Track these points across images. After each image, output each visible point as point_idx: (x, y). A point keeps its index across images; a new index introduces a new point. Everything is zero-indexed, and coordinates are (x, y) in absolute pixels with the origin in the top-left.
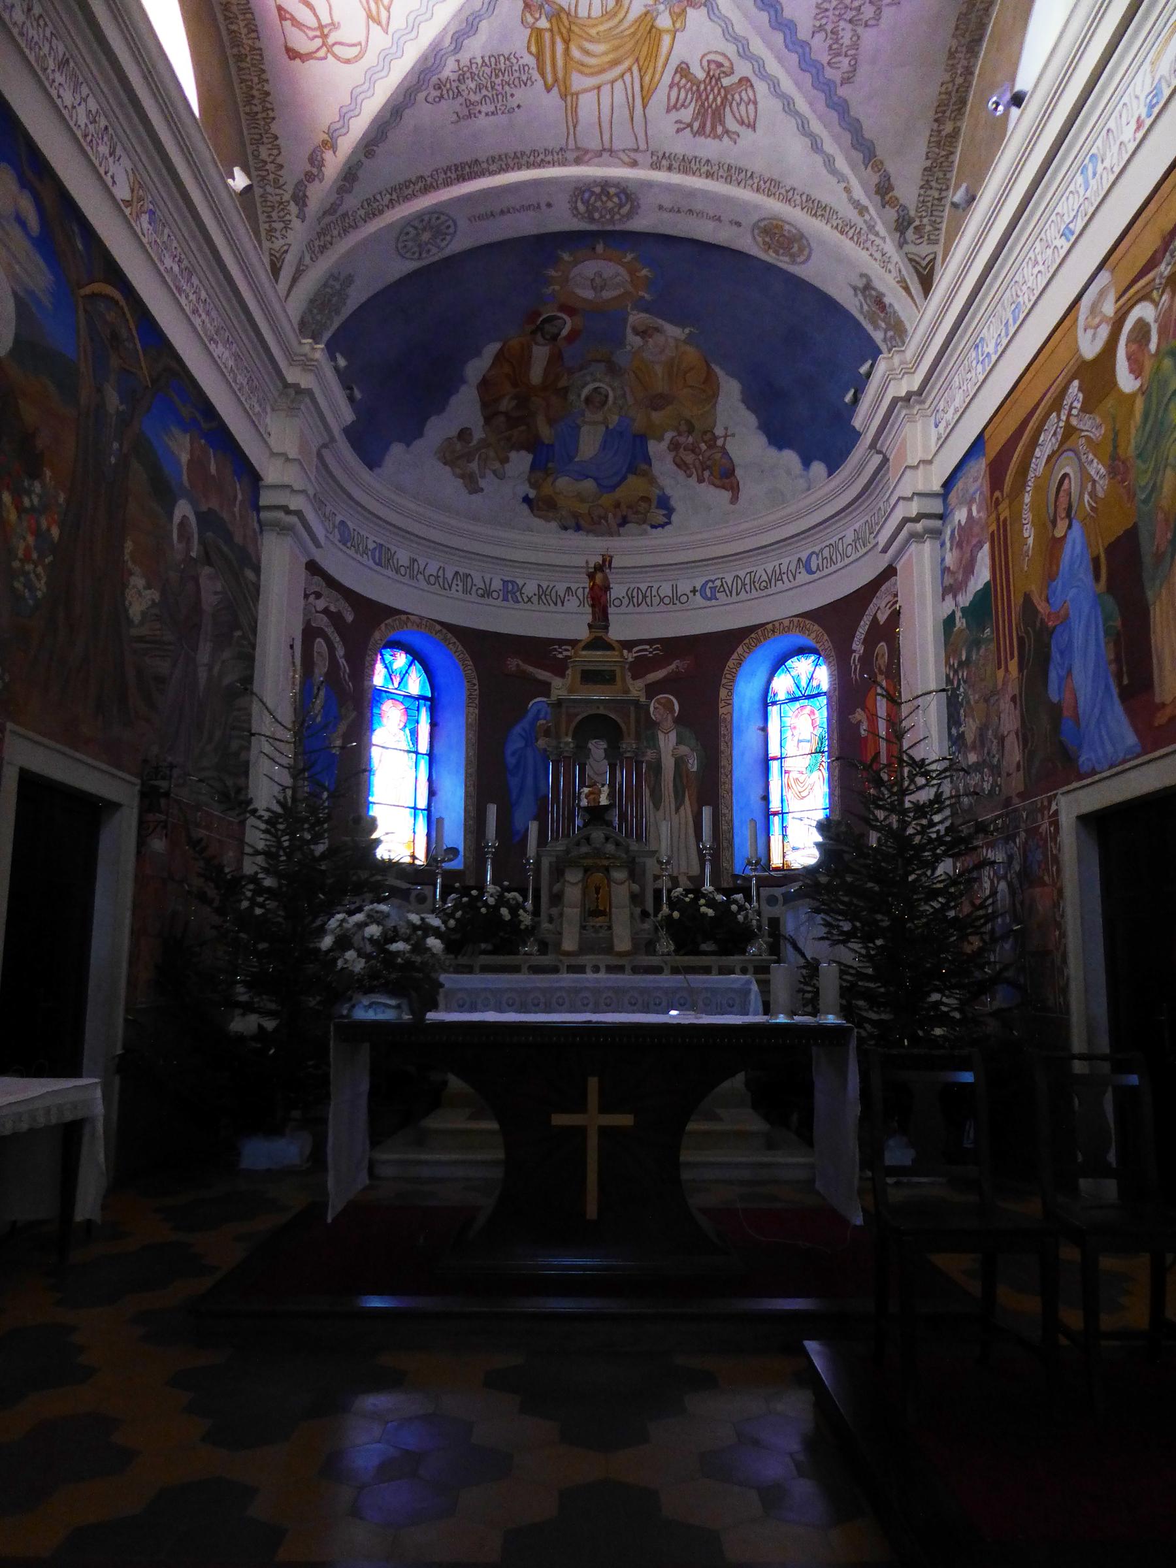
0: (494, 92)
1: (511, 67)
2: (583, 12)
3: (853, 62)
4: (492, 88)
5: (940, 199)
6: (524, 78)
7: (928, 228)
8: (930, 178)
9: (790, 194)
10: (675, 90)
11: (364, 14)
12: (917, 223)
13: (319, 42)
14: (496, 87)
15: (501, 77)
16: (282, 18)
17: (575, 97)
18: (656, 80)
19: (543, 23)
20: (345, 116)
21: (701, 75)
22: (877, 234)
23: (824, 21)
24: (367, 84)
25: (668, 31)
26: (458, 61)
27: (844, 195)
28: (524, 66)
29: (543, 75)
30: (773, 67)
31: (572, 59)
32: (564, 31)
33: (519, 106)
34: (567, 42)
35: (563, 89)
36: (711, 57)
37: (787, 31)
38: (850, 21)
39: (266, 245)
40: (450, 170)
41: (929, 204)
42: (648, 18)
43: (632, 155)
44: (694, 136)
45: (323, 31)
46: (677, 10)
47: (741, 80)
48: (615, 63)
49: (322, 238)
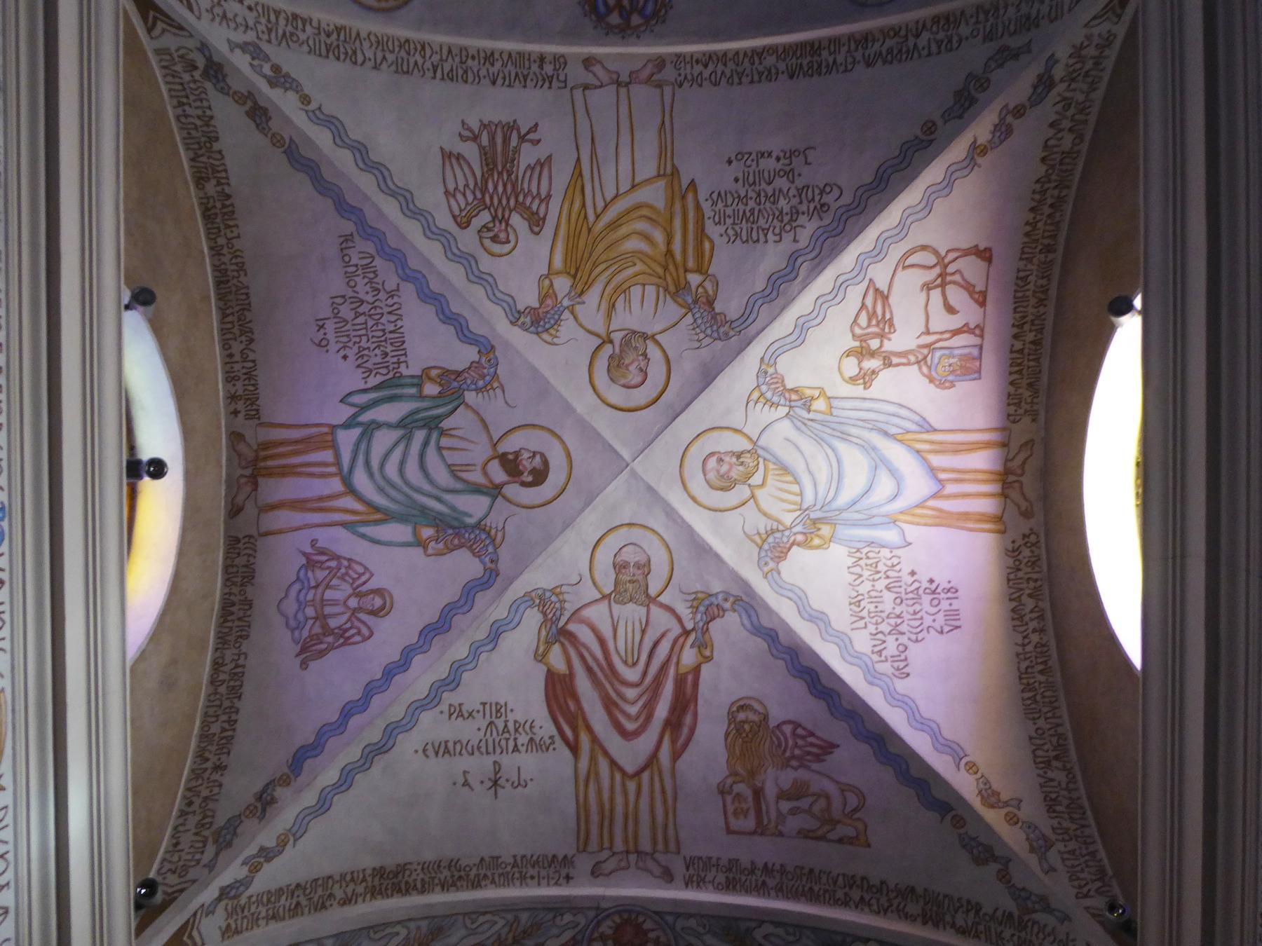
0: (757, 188)
1: (734, 223)
2: (651, 290)
3: (347, 259)
4: (759, 195)
5: (181, 104)
6: (720, 205)
7: (178, 68)
8: (205, 129)
9: (379, 55)
10: (543, 194)
11: (891, 300)
12: (197, 74)
13: (951, 269)
14: (754, 195)
15: (748, 209)
16: (984, 294)
17: (662, 172)
18: (566, 207)
19: (694, 279)
20: (948, 184)
21: (516, 219)
22: (244, 47)
23: (390, 301)
24: (908, 222)
25: (558, 273)
26: (795, 241)
27: (307, 90)
28: (719, 222)
29: (698, 206)
30: (432, 251)
31: (665, 229)
32: (671, 267)
33: (730, 162)
34: (669, 253)
35: (676, 183)
36: (507, 248)
37: (426, 291)
38: (362, 302)
39: (1121, 30)
40: (828, 66)
41: (192, 97)
42: (579, 290)
43: (590, 79)
44: (515, 121)
45: (943, 281)
46: (549, 302)
47: (468, 224)
48: (614, 225)
49: (1034, 15)
